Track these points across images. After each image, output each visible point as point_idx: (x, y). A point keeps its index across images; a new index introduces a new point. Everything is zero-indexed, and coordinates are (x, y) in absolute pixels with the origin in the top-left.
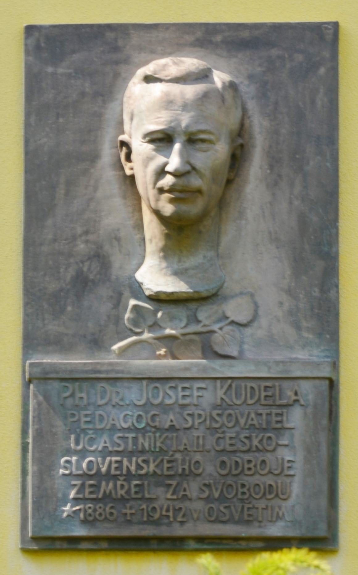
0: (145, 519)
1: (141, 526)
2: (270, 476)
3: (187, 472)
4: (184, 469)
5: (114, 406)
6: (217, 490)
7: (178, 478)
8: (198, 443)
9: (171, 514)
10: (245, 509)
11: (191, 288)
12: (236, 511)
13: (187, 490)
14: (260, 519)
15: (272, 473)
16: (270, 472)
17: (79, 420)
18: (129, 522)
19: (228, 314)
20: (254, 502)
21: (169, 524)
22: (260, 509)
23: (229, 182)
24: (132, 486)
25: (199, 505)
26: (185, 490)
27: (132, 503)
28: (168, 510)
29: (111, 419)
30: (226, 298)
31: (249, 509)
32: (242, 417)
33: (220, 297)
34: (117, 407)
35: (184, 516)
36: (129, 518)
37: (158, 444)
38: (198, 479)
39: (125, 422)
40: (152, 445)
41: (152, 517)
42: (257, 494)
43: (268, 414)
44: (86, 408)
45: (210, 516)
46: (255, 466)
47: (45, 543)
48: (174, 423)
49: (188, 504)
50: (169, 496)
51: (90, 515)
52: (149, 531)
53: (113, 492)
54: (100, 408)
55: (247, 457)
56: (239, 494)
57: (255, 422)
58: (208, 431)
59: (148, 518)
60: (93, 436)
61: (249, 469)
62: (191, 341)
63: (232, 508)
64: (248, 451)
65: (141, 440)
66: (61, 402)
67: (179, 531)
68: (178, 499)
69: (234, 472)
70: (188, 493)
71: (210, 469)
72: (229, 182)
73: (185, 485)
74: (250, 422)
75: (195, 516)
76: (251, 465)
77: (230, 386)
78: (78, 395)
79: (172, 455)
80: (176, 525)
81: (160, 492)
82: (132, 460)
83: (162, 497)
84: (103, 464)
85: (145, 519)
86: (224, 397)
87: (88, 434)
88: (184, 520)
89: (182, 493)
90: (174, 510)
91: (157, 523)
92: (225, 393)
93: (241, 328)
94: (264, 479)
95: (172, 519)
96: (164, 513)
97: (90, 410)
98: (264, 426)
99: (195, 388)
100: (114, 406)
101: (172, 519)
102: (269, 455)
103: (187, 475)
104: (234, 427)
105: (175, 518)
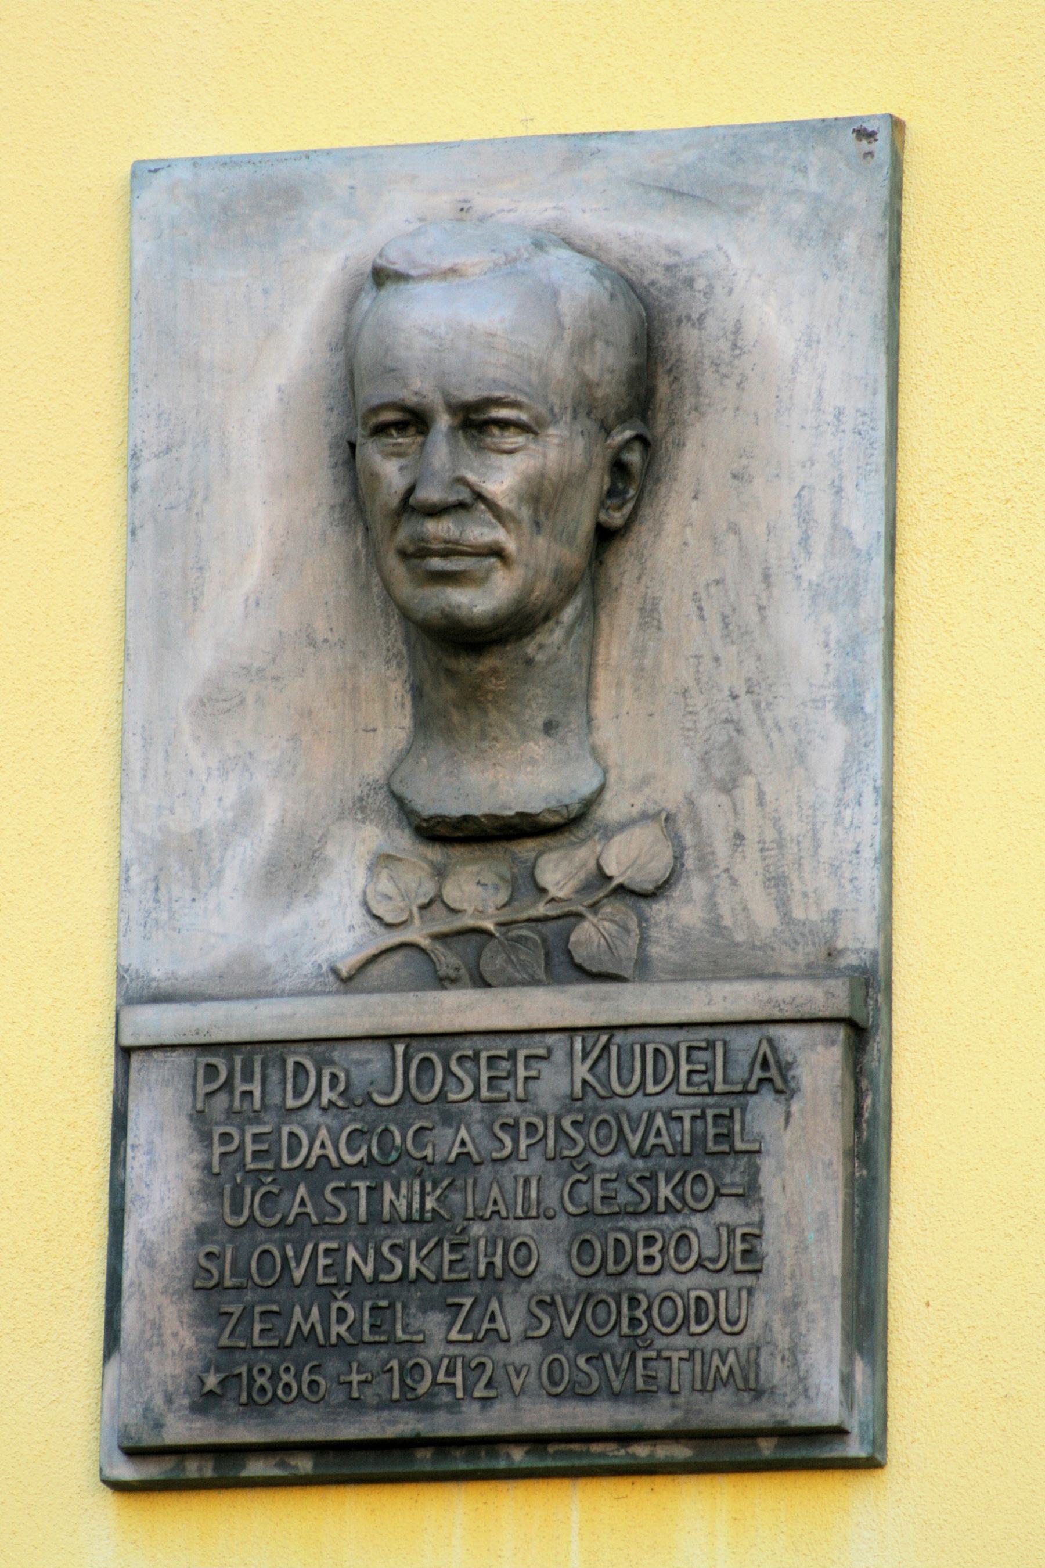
0: (396, 1395)
1: (385, 1414)
2: (700, 1273)
3: (499, 1272)
4: (490, 1265)
5: (324, 1110)
6: (569, 1318)
7: (475, 1287)
8: (526, 1198)
9: (458, 1380)
10: (639, 1363)
11: (640, 907)
12: (617, 1370)
13: (499, 1317)
14: (675, 1387)
15: (704, 1267)
16: (699, 1264)
17: (241, 1147)
18: (356, 1405)
19: (611, 870)
20: (660, 1342)
21: (454, 1407)
22: (675, 1361)
23: (605, 537)
24: (248, 1139)
25: (528, 1354)
26: (493, 1318)
27: (363, 1354)
28: (450, 1373)
29: (318, 1143)
30: (608, 832)
31: (646, 1360)
32: (634, 1132)
33: (591, 827)
34: (334, 1110)
35: (489, 1385)
36: (355, 1395)
37: (429, 1205)
38: (526, 1288)
39: (352, 1151)
40: (416, 1206)
41: (414, 1389)
42: (668, 1324)
43: (694, 1118)
44: (256, 1118)
45: (554, 1383)
46: (663, 1251)
47: (158, 1467)
48: (470, 1148)
49: (500, 1352)
50: (454, 1335)
51: (262, 1390)
52: (405, 1424)
53: (319, 1329)
54: (293, 1117)
55: (642, 1226)
56: (625, 1322)
57: (665, 1140)
58: (551, 1167)
59: (402, 1392)
60: (275, 1190)
61: (649, 1259)
62: (520, 939)
63: (608, 1359)
64: (652, 1210)
65: (388, 1194)
66: (199, 1106)
67: (477, 1422)
68: (475, 1340)
69: (611, 1268)
70: (500, 1325)
71: (554, 1263)
72: (605, 537)
73: (494, 1305)
74: (652, 1140)
75: (517, 1383)
76: (654, 1250)
77: (606, 1047)
78: (240, 1087)
79: (464, 1230)
80: (472, 1409)
81: (434, 1323)
82: (233, 1060)
83: (435, 1333)
84: (298, 1260)
85: (396, 1395)
86: (590, 1078)
87: (263, 1184)
88: (492, 1393)
89: (486, 1326)
90: (466, 1366)
91: (424, 1405)
92: (591, 1069)
93: (643, 904)
94: (684, 1283)
95: (460, 1394)
96: (441, 1378)
97: (265, 1123)
98: (687, 1149)
99: (521, 1055)
100: (324, 1110)
101: (460, 1394)
102: (697, 1221)
103: (500, 1280)
104: (612, 1152)
105: (468, 1390)
